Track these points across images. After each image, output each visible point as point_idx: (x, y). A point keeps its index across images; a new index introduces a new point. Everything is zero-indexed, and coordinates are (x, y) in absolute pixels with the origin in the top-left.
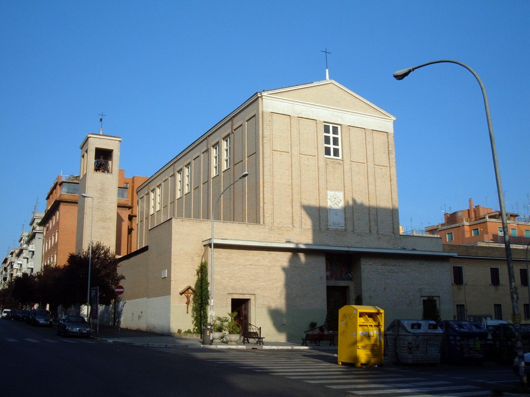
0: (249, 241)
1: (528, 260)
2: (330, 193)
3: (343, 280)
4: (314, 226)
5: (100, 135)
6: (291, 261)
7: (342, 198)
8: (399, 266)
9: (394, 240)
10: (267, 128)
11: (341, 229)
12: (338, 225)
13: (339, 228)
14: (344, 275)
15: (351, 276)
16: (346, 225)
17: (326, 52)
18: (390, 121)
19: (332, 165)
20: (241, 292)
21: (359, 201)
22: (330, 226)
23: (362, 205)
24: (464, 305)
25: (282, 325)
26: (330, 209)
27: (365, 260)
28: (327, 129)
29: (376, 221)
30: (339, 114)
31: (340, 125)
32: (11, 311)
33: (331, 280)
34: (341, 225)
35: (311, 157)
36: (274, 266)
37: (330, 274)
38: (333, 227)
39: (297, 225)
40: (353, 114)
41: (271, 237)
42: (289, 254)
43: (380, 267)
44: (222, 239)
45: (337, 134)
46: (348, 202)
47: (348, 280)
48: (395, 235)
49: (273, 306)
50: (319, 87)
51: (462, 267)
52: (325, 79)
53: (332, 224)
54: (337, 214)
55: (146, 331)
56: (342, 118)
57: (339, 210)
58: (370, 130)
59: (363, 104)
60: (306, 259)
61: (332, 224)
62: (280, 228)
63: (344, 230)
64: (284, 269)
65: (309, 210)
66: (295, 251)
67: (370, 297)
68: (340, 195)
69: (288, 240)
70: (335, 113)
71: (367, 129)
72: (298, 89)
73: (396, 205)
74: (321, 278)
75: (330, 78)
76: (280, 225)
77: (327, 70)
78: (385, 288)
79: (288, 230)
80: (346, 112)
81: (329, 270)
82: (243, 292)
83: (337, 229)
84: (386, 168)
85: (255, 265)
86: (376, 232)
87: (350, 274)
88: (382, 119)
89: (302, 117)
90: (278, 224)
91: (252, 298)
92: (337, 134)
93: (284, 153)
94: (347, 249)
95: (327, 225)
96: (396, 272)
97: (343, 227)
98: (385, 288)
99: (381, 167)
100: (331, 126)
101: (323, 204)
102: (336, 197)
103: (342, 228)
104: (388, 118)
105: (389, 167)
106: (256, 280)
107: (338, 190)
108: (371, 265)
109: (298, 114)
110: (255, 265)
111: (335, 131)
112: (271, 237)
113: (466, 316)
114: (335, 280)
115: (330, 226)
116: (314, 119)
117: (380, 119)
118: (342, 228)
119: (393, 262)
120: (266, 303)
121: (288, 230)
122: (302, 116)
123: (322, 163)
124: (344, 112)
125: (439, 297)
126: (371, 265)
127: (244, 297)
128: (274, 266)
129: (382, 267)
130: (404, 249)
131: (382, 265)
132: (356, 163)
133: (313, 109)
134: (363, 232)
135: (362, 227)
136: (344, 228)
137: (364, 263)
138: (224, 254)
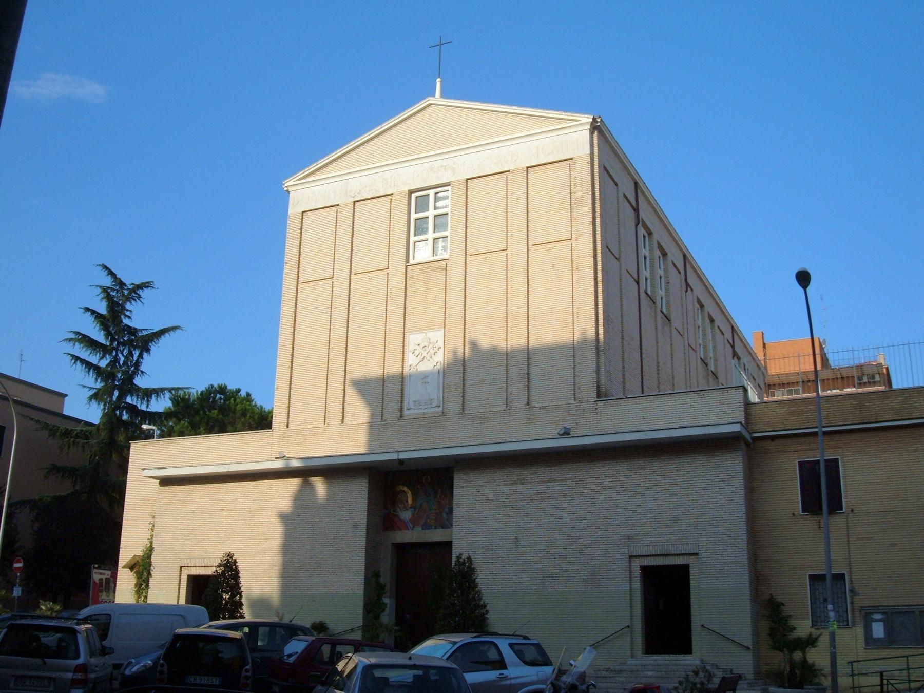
1: (824, 429)
3: (442, 528)
4: (373, 415)
6: (298, 498)
8: (562, 481)
11: (434, 413)
13: (429, 410)
14: (445, 516)
18: (581, 128)
20: (201, 562)
21: (485, 343)
23: (493, 352)
24: (843, 575)
27: (465, 477)
32: (41, 599)
34: (435, 404)
35: (376, 274)
42: (293, 484)
43: (505, 488)
48: (581, 402)
51: (838, 459)
52: (434, 96)
60: (329, 489)
61: (412, 406)
63: (440, 414)
65: (363, 387)
66: (305, 473)
68: (437, 336)
72: (358, 147)
74: (355, 526)
77: (438, 79)
79: (315, 434)
80: (461, 153)
81: (411, 508)
82: (204, 563)
83: (424, 414)
85: (229, 510)
86: (525, 405)
90: (299, 425)
93: (319, 283)
96: (551, 498)
97: (439, 406)
99: (549, 246)
101: (393, 368)
103: (437, 409)
104: (575, 123)
106: (229, 539)
107: (433, 327)
108: (482, 486)
109: (354, 197)
110: (229, 510)
113: (853, 609)
114: (423, 529)
115: (408, 409)
117: (551, 134)
118: (437, 409)
119: (543, 473)
121: (315, 434)
122: (363, 197)
124: (458, 154)
125: (181, 567)
126: (482, 486)
127: (208, 572)
129: (514, 488)
131: (513, 484)
134: (488, 410)
136: (441, 409)
137: (461, 484)
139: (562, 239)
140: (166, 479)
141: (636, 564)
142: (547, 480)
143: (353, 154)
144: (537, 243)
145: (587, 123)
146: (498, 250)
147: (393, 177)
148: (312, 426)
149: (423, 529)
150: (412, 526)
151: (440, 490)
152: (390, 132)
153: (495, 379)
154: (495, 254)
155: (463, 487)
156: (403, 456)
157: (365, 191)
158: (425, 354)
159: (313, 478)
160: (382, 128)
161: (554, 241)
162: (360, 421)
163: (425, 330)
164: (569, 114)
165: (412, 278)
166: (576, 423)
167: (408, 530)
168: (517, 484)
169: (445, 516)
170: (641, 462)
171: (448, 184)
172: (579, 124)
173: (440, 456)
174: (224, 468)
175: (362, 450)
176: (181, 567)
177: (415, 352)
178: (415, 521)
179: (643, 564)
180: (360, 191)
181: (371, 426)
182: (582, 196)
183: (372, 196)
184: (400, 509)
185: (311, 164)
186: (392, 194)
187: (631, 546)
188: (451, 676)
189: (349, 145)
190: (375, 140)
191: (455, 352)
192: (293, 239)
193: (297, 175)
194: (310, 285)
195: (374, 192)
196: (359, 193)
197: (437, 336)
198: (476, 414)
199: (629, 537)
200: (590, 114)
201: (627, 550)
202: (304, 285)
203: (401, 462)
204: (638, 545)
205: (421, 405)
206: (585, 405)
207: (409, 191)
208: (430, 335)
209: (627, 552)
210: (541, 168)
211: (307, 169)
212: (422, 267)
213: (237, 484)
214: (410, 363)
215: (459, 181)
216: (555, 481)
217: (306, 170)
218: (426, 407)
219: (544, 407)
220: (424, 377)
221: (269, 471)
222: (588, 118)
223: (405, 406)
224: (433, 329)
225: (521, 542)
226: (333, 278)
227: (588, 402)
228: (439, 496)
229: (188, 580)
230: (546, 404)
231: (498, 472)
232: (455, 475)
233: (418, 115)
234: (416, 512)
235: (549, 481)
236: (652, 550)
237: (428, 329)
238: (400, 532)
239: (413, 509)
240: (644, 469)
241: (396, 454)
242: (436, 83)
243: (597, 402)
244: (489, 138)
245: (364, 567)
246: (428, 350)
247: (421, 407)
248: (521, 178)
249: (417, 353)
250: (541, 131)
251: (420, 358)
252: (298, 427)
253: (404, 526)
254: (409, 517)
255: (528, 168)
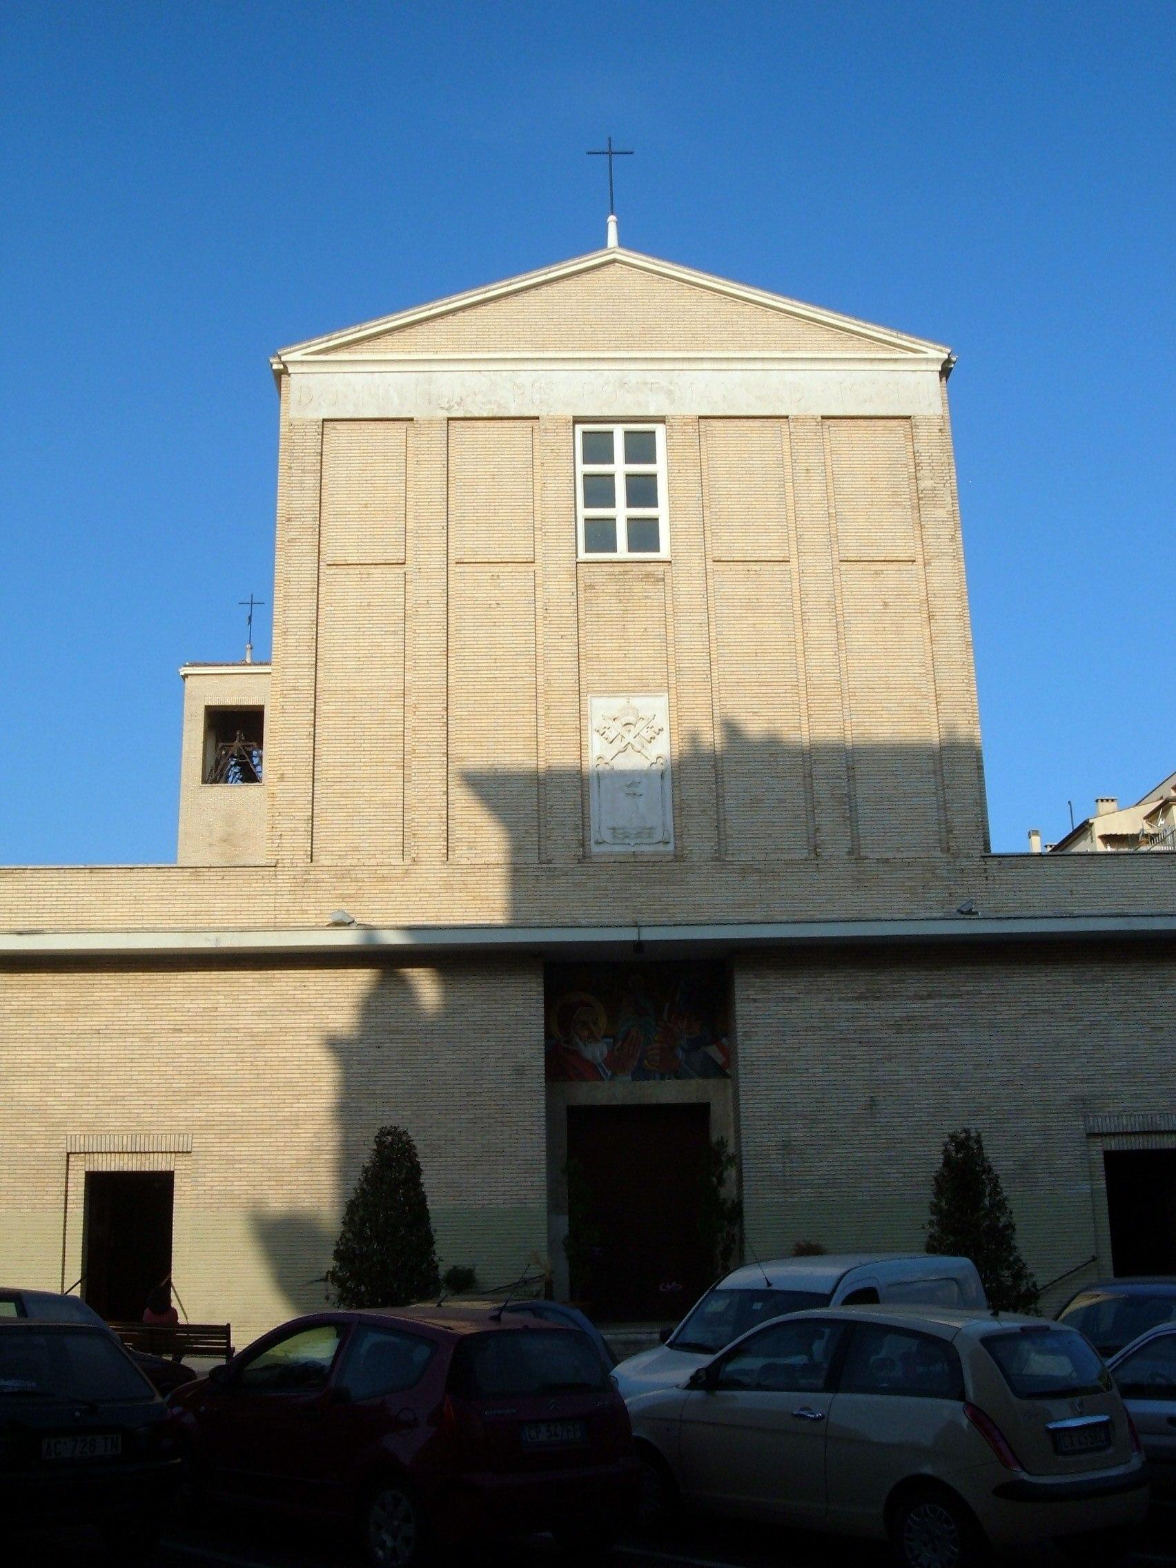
0: (136, 931)
2: (601, 708)
3: (678, 1078)
4: (517, 850)
5: (246, 664)
6: (370, 1007)
7: (662, 721)
8: (954, 996)
9: (949, 879)
10: (302, 482)
11: (657, 854)
12: (638, 835)
13: (645, 848)
14: (680, 1054)
15: (719, 1058)
16: (678, 836)
17: (610, 153)
18: (924, 367)
19: (612, 588)
21: (755, 727)
22: (597, 843)
23: (772, 747)
25: (312, 1282)
26: (599, 776)
28: (598, 448)
29: (848, 802)
30: (649, 377)
31: (661, 420)
33: (612, 1078)
34: (658, 836)
36: (284, 1030)
37: (605, 1050)
38: (617, 848)
39: (431, 850)
40: (724, 366)
41: (304, 912)
42: (359, 980)
43: (844, 1006)
44: (20, 933)
45: (652, 459)
46: (694, 739)
47: (704, 1075)
48: (956, 856)
49: (277, 1202)
50: (557, 287)
53: (607, 835)
54: (638, 790)
55: (764, 1286)
56: (670, 393)
57: (645, 775)
58: (813, 418)
59: (776, 321)
60: (447, 991)
61: (607, 835)
62: (344, 874)
63: (669, 858)
64: (335, 1045)
67: (786, 1146)
68: (656, 707)
69: (338, 917)
70: (633, 378)
71: (796, 419)
73: (968, 727)
74: (519, 1072)
75: (622, 243)
76: (348, 862)
77: (612, 218)
78: (873, 1103)
79: (384, 879)
80: (686, 366)
81: (605, 1036)
83: (634, 854)
84: (902, 568)
87: (713, 1051)
88: (875, 366)
89: (469, 415)
91: (180, 1167)
92: (652, 459)
93: (372, 570)
94: (629, 935)
95: (583, 843)
96: (934, 1027)
98: (873, 1103)
99: (873, 568)
100: (619, 431)
101: (559, 757)
102: (631, 719)
103: (661, 848)
104: (911, 355)
105: (920, 561)
107: (642, 687)
111: (641, 447)
112: (304, 912)
114: (635, 1078)
115: (597, 843)
116: (526, 415)
117: (868, 366)
118: (661, 848)
119: (916, 981)
120: (239, 1187)
121: (384, 879)
122: (471, 412)
123: (559, 587)
124: (678, 366)
125: (68, 1154)
128: (284, 1030)
129: (861, 1005)
130: (968, 914)
131: (858, 999)
132: (741, 566)
133: (525, 378)
135: (770, 836)
136: (671, 847)
137: (752, 993)
138: (56, 992)
139: (899, 559)
140: (124, 956)
141: (1097, 1149)
142: (925, 993)
143: (440, 324)
144: (723, 559)
145: (938, 359)
146: (772, 559)
147: (537, 385)
148: (373, 862)
149: (635, 1078)
150: (609, 1073)
151: (667, 1005)
152: (524, 297)
153: (782, 801)
154: (769, 567)
155: (755, 1001)
156: (649, 935)
157: (474, 402)
158: (629, 738)
159: (410, 970)
160: (510, 284)
161: (883, 559)
162: (492, 860)
163: (626, 691)
164: (904, 337)
165: (591, 587)
166: (950, 893)
167: (602, 1079)
168: (866, 998)
169: (680, 1054)
170: (1097, 970)
171: (661, 420)
172: (924, 359)
173: (757, 939)
174: (207, 939)
175: (499, 918)
176: (68, 1154)
177: (608, 732)
178: (616, 1064)
179: (1109, 1149)
180: (461, 399)
181: (516, 870)
182: (934, 489)
183: (491, 415)
184: (581, 1039)
185: (346, 327)
186: (537, 418)
187: (1089, 1117)
188: (249, 1367)
189: (435, 305)
190: (491, 306)
191: (694, 739)
192: (303, 471)
193: (313, 342)
194: (352, 572)
195: (495, 407)
196: (459, 404)
197: (656, 707)
198: (748, 863)
199: (1083, 1100)
200: (946, 345)
201: (1082, 1123)
202: (333, 570)
203: (639, 946)
204: (1100, 1114)
205: (628, 837)
206: (964, 863)
207: (574, 417)
208: (639, 702)
209: (1082, 1127)
210: (758, 423)
211: (337, 335)
212: (611, 569)
213: (214, 975)
214: (596, 754)
215: (684, 417)
216: (940, 996)
217: (334, 336)
218: (639, 841)
219: (886, 861)
220: (631, 782)
221: (322, 950)
222: (941, 351)
223: (593, 836)
224: (646, 691)
225: (880, 1107)
226: (404, 564)
227: (968, 857)
228: (665, 1016)
229: (86, 1178)
230: (889, 855)
231: (826, 975)
232: (736, 976)
233: (585, 277)
234: (618, 1046)
235: (929, 996)
236: (1125, 1123)
237: (634, 692)
238: (584, 1084)
239: (611, 1040)
240: (1103, 981)
241: (636, 930)
242: (606, 226)
243: (986, 859)
244: (741, 349)
245: (544, 1153)
246: (634, 731)
247: (627, 841)
248: (438, 434)
249: (611, 734)
250: (661, 356)
251: (619, 745)
252: (339, 863)
253: (591, 1072)
254: (601, 1054)
255: (324, 420)
